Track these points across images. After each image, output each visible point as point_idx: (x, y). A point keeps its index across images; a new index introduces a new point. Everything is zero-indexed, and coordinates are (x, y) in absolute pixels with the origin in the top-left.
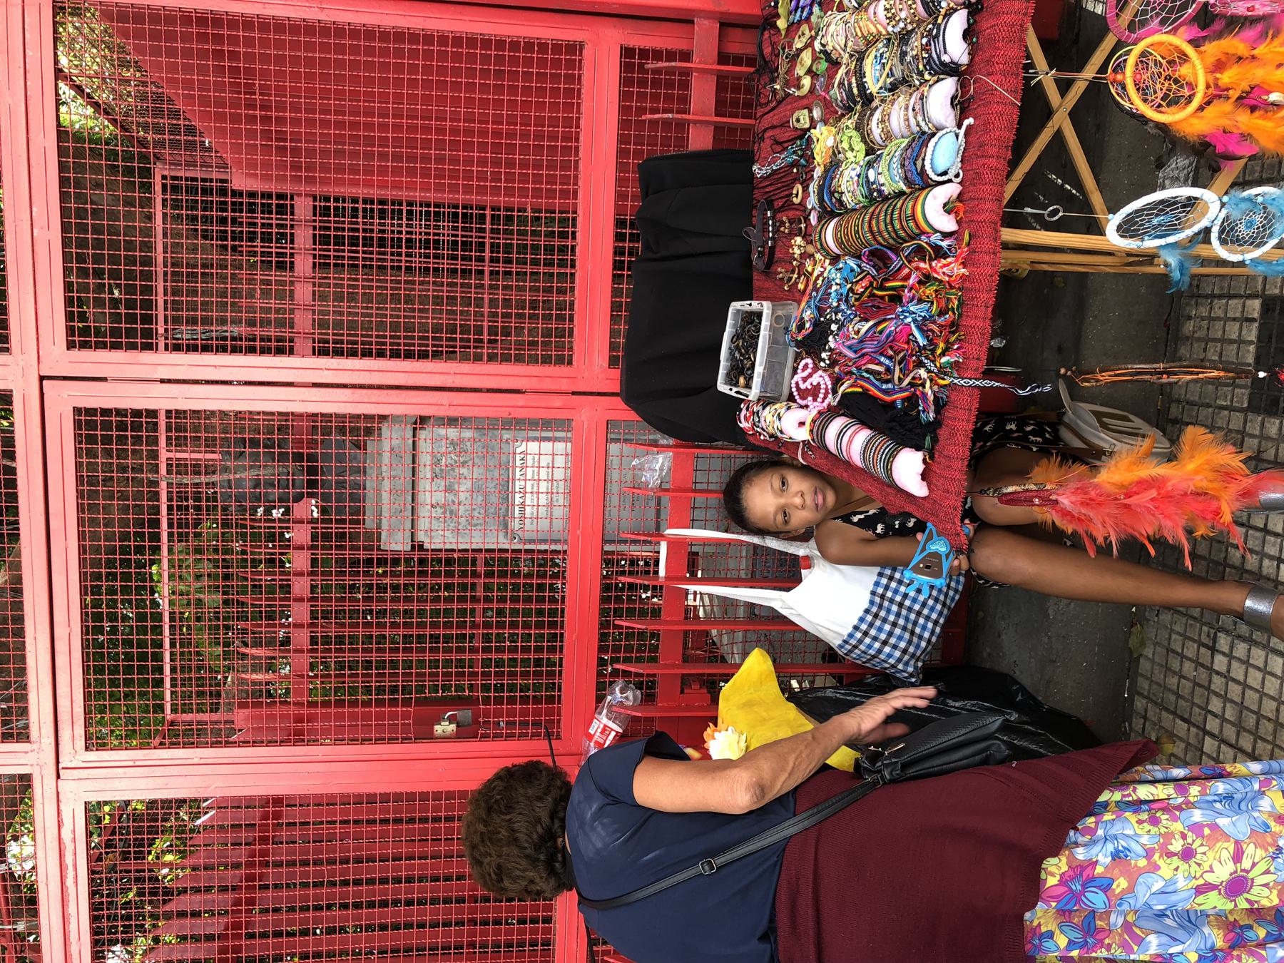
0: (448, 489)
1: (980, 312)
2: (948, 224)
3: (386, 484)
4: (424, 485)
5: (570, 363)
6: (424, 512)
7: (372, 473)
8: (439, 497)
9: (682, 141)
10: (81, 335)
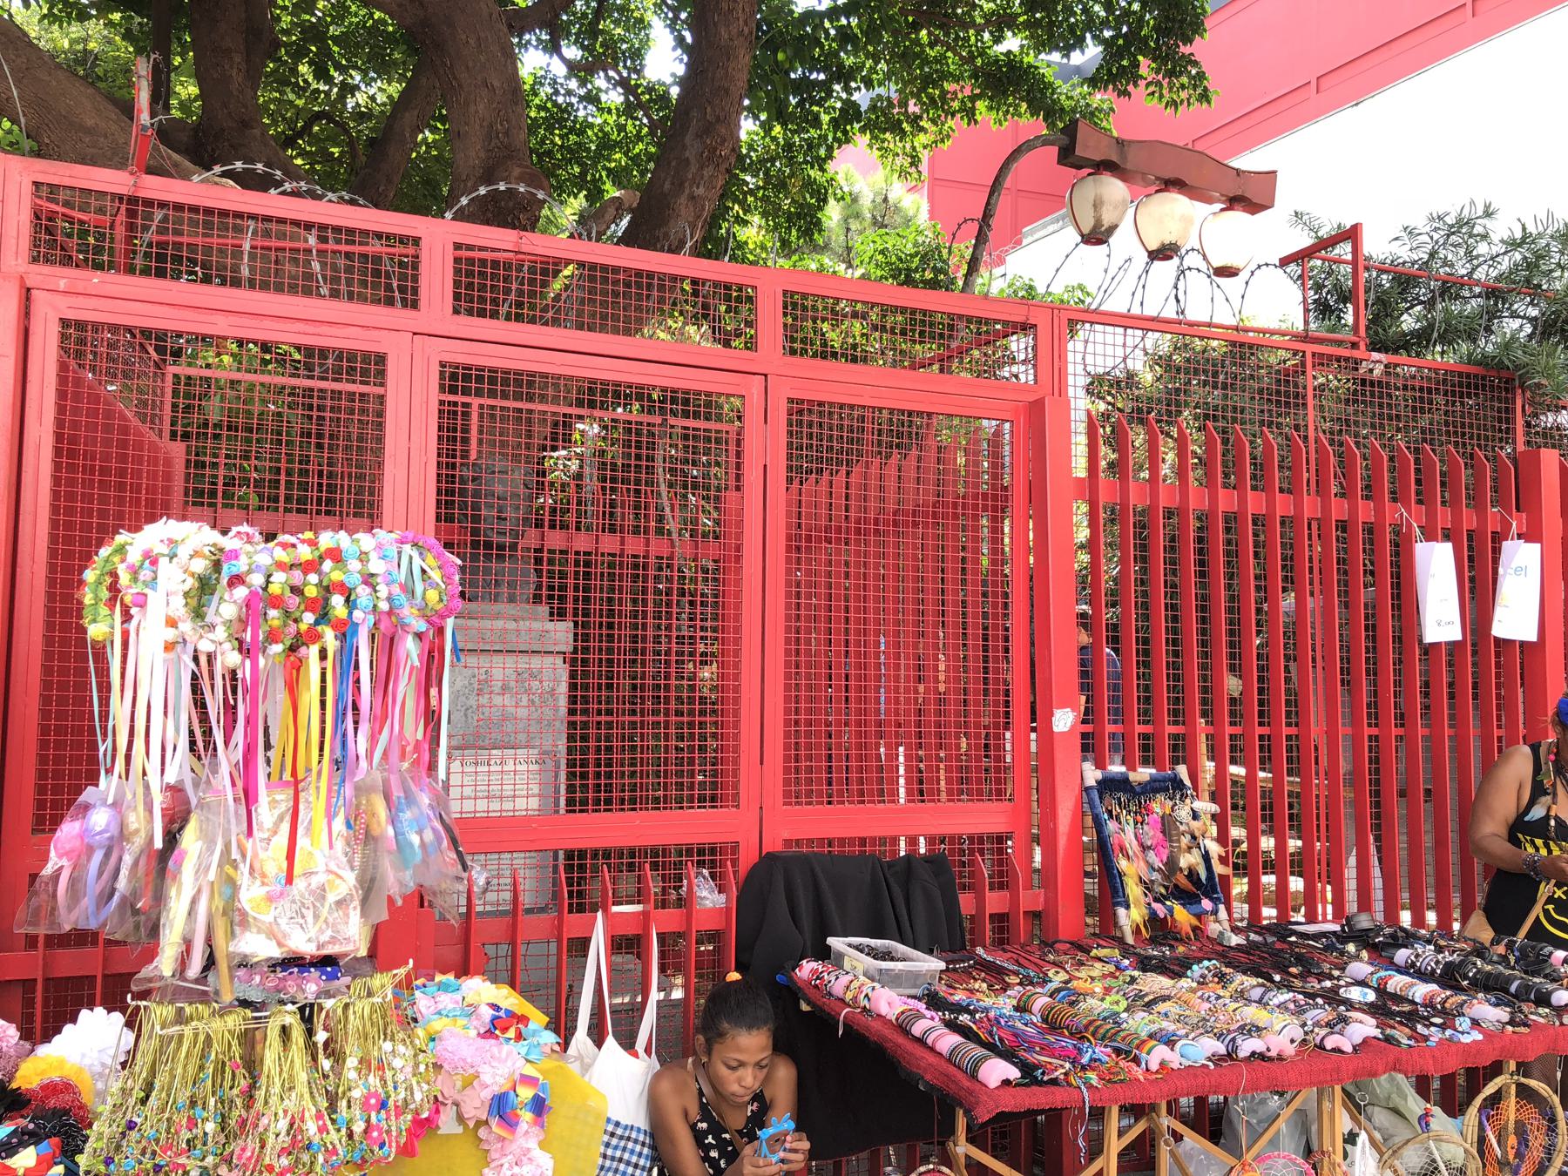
0: (505, 689)
1: (1128, 1094)
2: (1154, 1066)
3: (512, 625)
4: (510, 660)
5: (785, 804)
6: (484, 661)
7: (511, 609)
8: (497, 674)
9: (963, 887)
10: (798, 409)
